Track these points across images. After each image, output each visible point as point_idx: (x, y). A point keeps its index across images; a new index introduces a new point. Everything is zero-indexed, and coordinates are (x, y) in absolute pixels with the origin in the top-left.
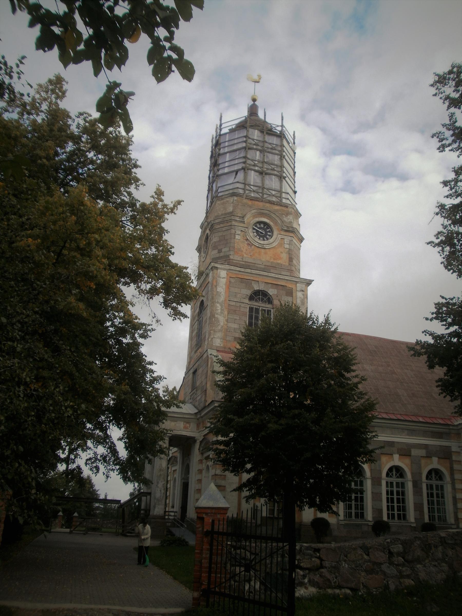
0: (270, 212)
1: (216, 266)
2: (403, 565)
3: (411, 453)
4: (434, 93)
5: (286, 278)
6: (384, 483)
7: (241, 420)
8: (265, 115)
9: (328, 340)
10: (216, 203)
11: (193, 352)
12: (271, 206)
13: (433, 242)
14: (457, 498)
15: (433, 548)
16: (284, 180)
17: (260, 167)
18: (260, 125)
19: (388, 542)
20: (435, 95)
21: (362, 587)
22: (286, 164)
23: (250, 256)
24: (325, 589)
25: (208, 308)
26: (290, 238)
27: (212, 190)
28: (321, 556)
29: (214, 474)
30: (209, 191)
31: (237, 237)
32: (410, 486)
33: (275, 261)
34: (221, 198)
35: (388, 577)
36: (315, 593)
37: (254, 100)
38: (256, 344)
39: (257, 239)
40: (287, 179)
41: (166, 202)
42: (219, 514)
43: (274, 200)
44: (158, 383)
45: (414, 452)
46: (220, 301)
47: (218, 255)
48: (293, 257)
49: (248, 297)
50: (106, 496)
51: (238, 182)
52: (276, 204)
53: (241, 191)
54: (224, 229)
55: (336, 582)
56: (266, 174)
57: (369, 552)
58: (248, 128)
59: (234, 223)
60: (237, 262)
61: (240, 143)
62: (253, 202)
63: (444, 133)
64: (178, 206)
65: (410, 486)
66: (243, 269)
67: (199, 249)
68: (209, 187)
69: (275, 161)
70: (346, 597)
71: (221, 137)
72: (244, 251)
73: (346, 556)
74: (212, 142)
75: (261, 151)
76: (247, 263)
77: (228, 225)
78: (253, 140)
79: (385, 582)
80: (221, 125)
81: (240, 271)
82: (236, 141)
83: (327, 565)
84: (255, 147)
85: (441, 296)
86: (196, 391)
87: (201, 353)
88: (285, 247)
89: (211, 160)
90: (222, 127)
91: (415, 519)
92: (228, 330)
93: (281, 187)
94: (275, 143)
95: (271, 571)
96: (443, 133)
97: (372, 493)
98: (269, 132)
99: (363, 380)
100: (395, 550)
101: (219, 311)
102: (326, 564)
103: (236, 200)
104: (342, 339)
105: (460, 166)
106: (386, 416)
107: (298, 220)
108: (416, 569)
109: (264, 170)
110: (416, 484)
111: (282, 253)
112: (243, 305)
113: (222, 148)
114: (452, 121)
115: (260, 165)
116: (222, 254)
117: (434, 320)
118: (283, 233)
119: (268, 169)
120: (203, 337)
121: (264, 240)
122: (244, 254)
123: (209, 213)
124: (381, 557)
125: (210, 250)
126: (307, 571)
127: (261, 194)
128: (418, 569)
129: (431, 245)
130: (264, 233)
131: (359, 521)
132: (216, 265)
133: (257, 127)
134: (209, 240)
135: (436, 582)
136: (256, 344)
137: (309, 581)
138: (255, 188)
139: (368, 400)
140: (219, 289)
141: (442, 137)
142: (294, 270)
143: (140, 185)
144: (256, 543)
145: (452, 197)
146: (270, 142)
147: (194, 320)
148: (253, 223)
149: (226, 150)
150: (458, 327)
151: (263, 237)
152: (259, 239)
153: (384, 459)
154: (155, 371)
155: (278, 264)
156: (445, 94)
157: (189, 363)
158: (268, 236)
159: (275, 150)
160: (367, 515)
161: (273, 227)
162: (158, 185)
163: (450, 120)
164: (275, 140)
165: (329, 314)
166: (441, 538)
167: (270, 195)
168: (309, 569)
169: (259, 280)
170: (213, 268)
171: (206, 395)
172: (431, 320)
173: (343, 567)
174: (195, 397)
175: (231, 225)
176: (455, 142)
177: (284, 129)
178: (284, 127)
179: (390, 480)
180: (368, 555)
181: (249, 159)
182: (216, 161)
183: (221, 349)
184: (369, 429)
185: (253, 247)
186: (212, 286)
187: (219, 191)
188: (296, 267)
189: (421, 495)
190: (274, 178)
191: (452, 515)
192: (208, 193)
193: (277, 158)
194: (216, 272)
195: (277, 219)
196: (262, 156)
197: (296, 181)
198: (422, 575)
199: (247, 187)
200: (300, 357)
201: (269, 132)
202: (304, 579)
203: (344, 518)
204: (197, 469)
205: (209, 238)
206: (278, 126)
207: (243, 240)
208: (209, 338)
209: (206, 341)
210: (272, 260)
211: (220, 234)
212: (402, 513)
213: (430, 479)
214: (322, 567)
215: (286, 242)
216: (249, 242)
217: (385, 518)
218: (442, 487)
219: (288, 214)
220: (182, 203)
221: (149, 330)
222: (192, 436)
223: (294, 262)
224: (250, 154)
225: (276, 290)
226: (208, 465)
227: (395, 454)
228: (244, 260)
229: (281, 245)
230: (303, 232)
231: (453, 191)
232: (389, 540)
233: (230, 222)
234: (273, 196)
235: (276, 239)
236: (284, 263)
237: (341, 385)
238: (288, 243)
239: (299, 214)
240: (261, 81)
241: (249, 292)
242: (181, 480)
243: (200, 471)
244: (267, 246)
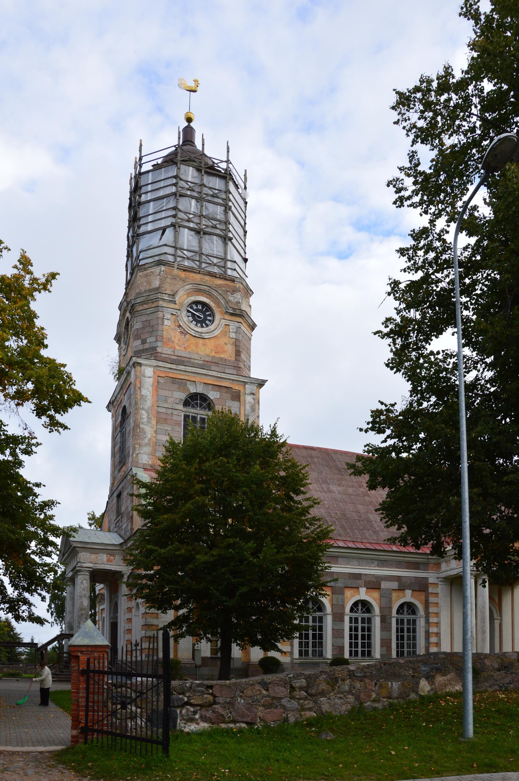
0: (210, 289)
1: (139, 362)
2: (305, 699)
4: (396, 120)
5: (232, 377)
6: (347, 619)
7: (163, 551)
8: (203, 145)
9: (274, 455)
10: (136, 274)
11: (117, 471)
12: (212, 279)
13: (381, 332)
15: (340, 681)
16: (229, 243)
17: (197, 224)
18: (196, 160)
19: (290, 677)
20: (397, 123)
21: (258, 720)
22: (232, 219)
23: (183, 349)
24: (218, 724)
25: (131, 416)
26: (238, 324)
27: (132, 257)
28: (214, 692)
29: (144, 612)
30: (128, 256)
31: (166, 322)
32: (377, 622)
33: (217, 355)
34: (144, 268)
35: (288, 711)
36: (206, 728)
37: (189, 120)
38: (181, 461)
39: (192, 325)
40: (234, 241)
41: (37, 275)
42: (96, 652)
43: (216, 271)
44: (50, 509)
45: (384, 585)
46: (146, 408)
47: (141, 347)
48: (241, 350)
49: (182, 402)
50: (32, 640)
51: (166, 245)
52: (219, 277)
53: (171, 258)
54: (149, 311)
55: (230, 717)
56: (205, 233)
57: (268, 688)
58: (179, 164)
59: (161, 303)
60: (167, 356)
61: (168, 187)
62: (188, 273)
63: (403, 179)
64: (53, 281)
65: (377, 622)
66: (174, 365)
67: (118, 339)
68: (128, 251)
69: (217, 214)
70: (240, 731)
71: (142, 177)
72: (176, 341)
73: (243, 692)
74: (130, 184)
75: (197, 199)
76: (179, 358)
77: (153, 305)
78: (187, 182)
79: (284, 715)
80: (141, 159)
81: (171, 368)
82: (162, 184)
83: (221, 701)
84: (189, 193)
85: (379, 401)
86: (122, 517)
87: (125, 472)
88: (231, 336)
89: (129, 212)
90: (142, 162)
91: (381, 655)
92: (158, 444)
93: (226, 253)
94: (217, 188)
95: (158, 709)
96: (401, 180)
97: (333, 629)
98: (209, 171)
99: (315, 503)
100: (297, 685)
101: (146, 420)
102: (220, 700)
103: (163, 271)
104: (291, 454)
105: (421, 228)
106: (353, 545)
107: (249, 299)
108: (319, 702)
109: (201, 227)
110: (385, 620)
111: (226, 344)
112: (175, 412)
113: (144, 193)
114: (413, 163)
115: (197, 220)
116: (147, 346)
117: (370, 431)
118: (227, 317)
119: (207, 226)
120: (127, 452)
121: (202, 327)
122: (176, 345)
123: (129, 289)
124: (281, 691)
125: (132, 340)
126: (198, 708)
127: (198, 263)
128: (321, 702)
129: (379, 336)
130: (202, 317)
131: (317, 660)
132: (139, 360)
133: (191, 163)
134: (130, 326)
135: (339, 713)
136: (181, 461)
137: (201, 717)
138: (189, 254)
139: (320, 527)
140: (144, 392)
141: (401, 186)
142: (243, 366)
143: (3, 250)
144: (99, 677)
145: (411, 270)
146: (211, 185)
147: (116, 431)
148: (188, 304)
149: (149, 196)
150: (397, 439)
151: (202, 322)
152: (196, 325)
153: (348, 593)
154: (39, 495)
155: (221, 359)
156: (409, 122)
157: (112, 484)
158: (207, 322)
159: (218, 197)
160: (326, 653)
161: (214, 308)
162: (23, 250)
163: (411, 161)
164: (217, 183)
165: (276, 423)
166: (350, 671)
167: (210, 264)
168: (201, 706)
169: (196, 380)
170: (136, 364)
171: (132, 522)
172: (366, 431)
173: (238, 703)
174: (121, 525)
175: (158, 306)
176: (417, 195)
177: (230, 166)
178: (231, 163)
179: (354, 615)
180: (267, 690)
181: (180, 211)
182: (136, 213)
183: (149, 468)
184: (321, 560)
185: (188, 336)
186: (135, 388)
187: (140, 258)
188: (246, 363)
189: (390, 630)
190: (216, 240)
192: (127, 261)
193: (220, 209)
194: (139, 370)
195: (219, 297)
196: (199, 207)
197: (246, 244)
198: (326, 707)
199: (179, 253)
200: (237, 476)
201: (209, 171)
202: (195, 715)
204: (126, 607)
205: (130, 324)
206: (222, 161)
207: (174, 327)
208: (133, 454)
209: (130, 458)
210: (213, 354)
211: (144, 318)
212: (366, 649)
213: (402, 614)
214: (215, 703)
215: (231, 330)
216: (182, 330)
217: (347, 656)
218: (414, 621)
219: (234, 291)
220: (57, 277)
221: (33, 444)
222: (118, 570)
223: (243, 356)
224: (184, 204)
225: (218, 393)
226: (138, 603)
227: (362, 587)
228: (176, 354)
229: (225, 333)
230: (255, 316)
231: (412, 262)
232: (291, 675)
233: (156, 301)
234: (215, 265)
235: (218, 326)
236: (229, 358)
237: (290, 509)
238: (235, 330)
239: (249, 291)
240: (198, 89)
241: (183, 396)
242: (110, 619)
243: (130, 610)
244: (207, 334)
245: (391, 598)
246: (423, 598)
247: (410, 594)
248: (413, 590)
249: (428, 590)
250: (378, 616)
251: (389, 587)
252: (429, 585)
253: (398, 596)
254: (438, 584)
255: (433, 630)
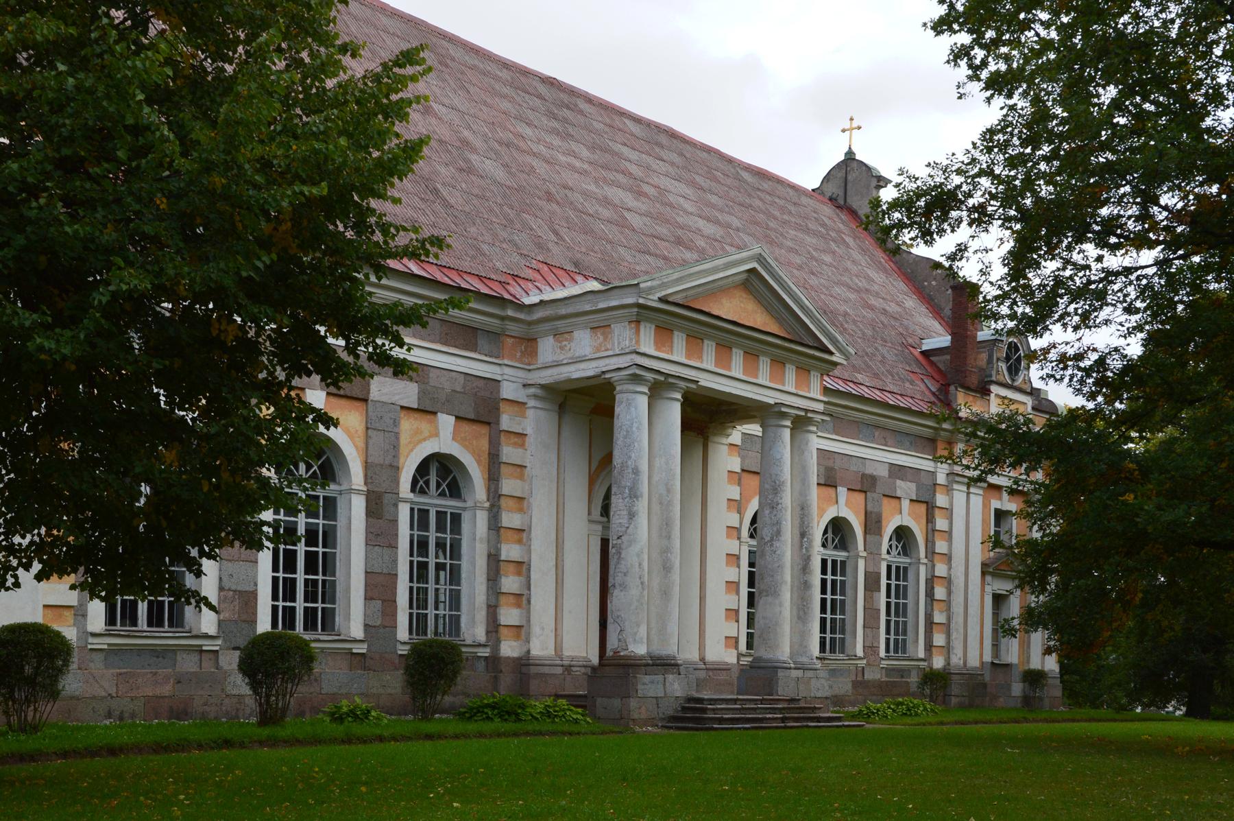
3: (368, 392)
6: (404, 513)
14: (503, 557)
91: (366, 626)
110: (378, 506)
160: (348, 617)
191: (481, 616)
203: (411, 632)
213: (423, 492)
218: (456, 519)
245: (397, 436)
246: (484, 444)
247: (451, 429)
248: (457, 417)
249: (498, 423)
250: (358, 492)
251: (395, 399)
252: (502, 406)
253: (417, 432)
254: (524, 404)
255: (510, 551)
